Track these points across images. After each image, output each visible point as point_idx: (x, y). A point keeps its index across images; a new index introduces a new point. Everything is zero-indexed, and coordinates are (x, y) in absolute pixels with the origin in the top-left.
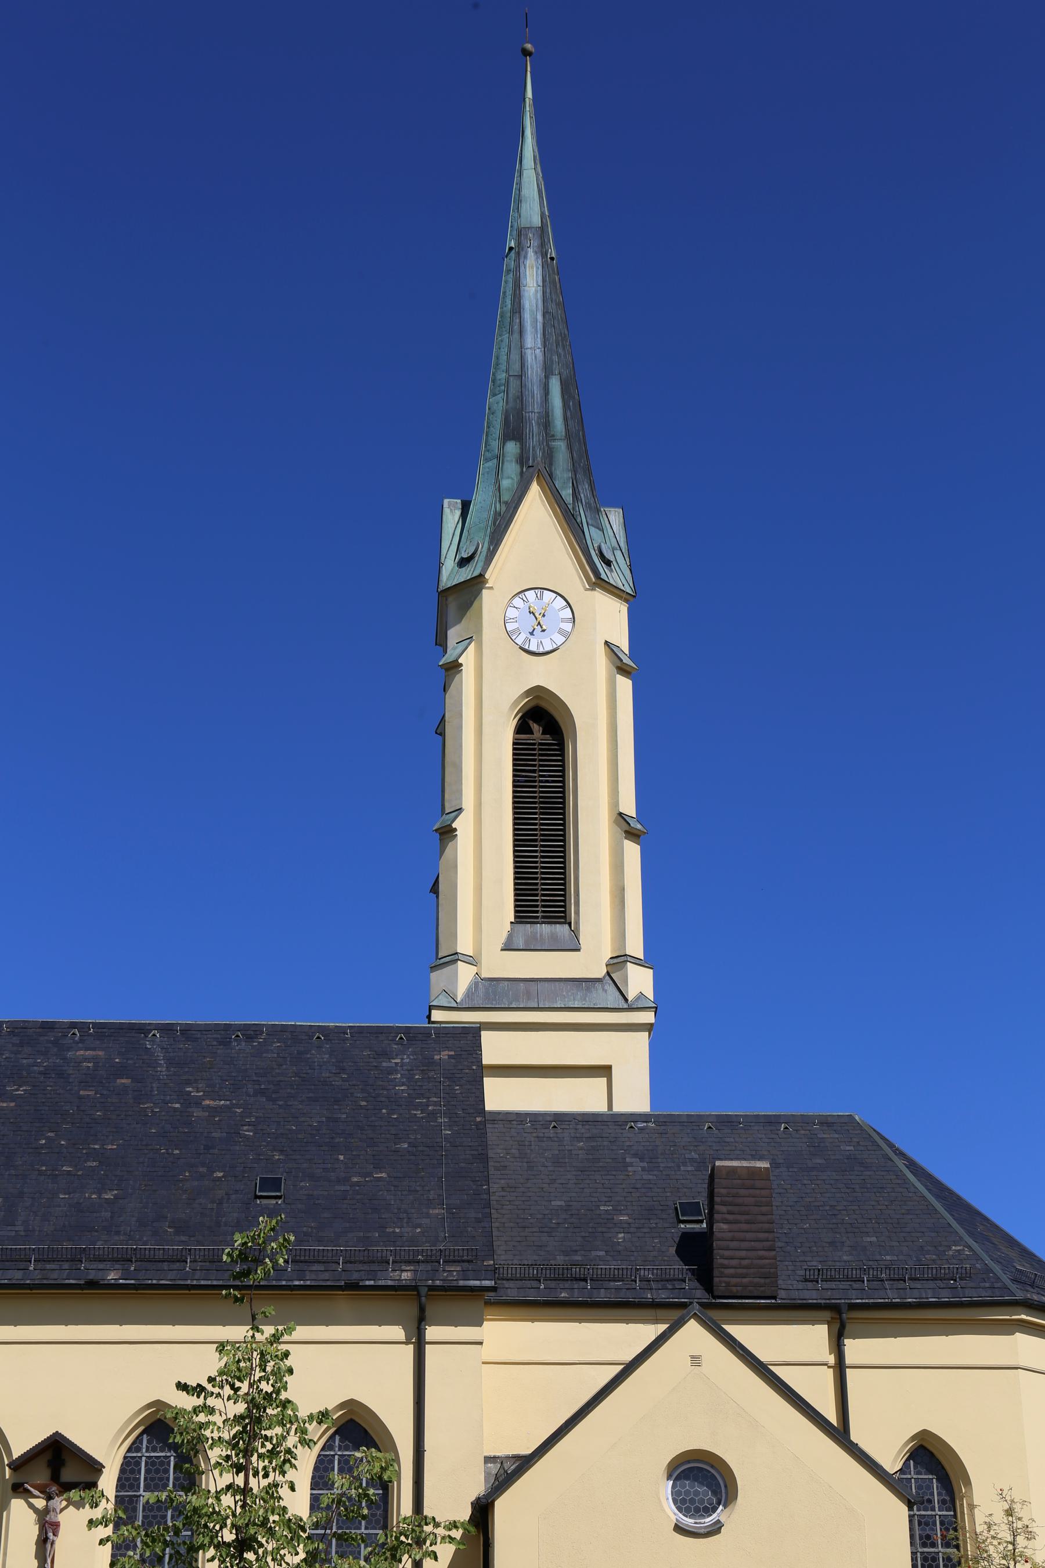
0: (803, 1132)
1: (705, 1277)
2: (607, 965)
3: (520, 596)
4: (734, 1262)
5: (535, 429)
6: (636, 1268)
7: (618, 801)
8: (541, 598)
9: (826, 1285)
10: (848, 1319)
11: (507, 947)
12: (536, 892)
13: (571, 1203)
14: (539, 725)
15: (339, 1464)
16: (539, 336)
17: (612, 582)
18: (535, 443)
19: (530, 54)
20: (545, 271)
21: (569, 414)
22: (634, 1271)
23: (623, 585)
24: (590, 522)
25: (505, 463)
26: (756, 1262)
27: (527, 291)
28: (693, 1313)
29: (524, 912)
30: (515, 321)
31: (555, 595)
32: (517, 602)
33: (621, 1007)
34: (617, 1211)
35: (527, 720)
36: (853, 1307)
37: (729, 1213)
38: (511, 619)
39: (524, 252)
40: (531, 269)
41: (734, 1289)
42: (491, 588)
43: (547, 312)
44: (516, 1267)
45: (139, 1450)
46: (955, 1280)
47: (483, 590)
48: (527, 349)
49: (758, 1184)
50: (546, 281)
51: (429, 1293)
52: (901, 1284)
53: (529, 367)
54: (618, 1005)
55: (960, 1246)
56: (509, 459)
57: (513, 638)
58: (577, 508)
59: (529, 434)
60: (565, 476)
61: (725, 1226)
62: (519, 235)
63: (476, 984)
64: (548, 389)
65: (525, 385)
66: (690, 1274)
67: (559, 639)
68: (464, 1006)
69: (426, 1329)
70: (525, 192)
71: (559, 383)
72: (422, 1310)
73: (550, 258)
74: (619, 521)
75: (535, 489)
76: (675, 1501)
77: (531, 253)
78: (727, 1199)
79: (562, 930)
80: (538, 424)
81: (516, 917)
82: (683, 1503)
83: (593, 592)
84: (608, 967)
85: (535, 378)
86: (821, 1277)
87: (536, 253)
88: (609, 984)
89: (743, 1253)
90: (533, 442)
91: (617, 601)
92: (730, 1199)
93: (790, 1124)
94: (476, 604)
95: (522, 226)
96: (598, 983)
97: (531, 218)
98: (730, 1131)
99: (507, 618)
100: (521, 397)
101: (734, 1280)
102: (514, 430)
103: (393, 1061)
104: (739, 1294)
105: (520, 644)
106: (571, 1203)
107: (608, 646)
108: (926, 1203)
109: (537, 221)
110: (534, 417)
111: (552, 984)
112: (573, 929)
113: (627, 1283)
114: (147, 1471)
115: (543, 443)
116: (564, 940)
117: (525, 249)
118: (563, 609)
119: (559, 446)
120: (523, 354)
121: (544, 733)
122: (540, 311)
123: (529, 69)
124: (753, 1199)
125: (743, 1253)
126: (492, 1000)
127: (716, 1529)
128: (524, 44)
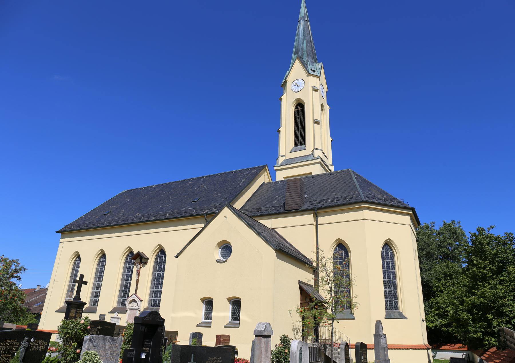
21: (307, 46)
29: (297, 144)
32: (294, 83)
36: (318, 209)
42: (288, 82)
49: (297, 182)
51: (207, 215)
67: (302, 88)
75: (297, 61)
76: (221, 255)
77: (302, 21)
79: (303, 146)
83: (308, 77)
87: (303, 20)
89: (292, 199)
101: (289, 206)
102: (296, 53)
111: (300, 158)
114: (159, 260)
125: (292, 199)
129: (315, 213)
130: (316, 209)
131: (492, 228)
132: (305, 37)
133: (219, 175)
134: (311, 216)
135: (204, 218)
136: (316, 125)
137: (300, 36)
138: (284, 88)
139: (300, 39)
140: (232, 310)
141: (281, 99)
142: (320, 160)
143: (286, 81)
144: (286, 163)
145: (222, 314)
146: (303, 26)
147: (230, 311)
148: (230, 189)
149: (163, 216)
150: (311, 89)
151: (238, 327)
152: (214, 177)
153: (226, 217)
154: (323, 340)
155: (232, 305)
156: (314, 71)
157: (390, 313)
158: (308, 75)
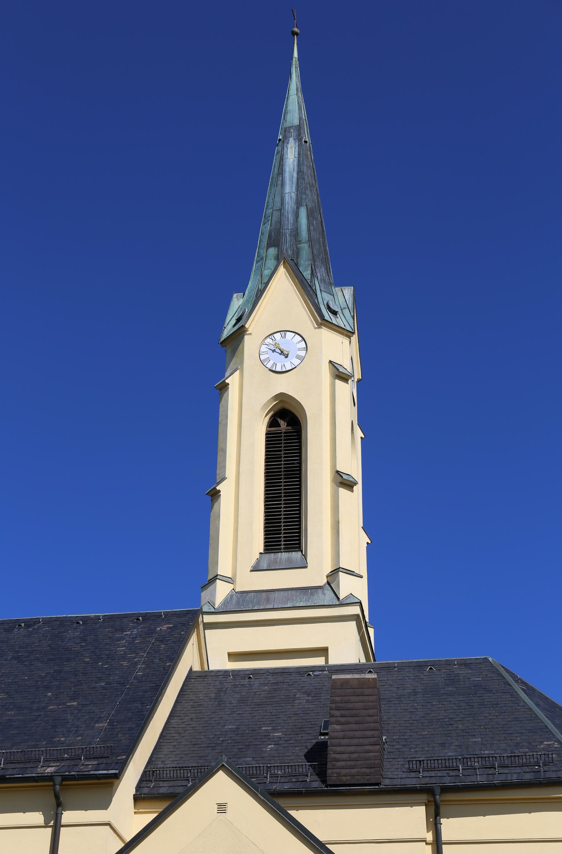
0: (444, 671)
1: (322, 774)
2: (327, 577)
3: (270, 337)
4: (344, 756)
5: (288, 238)
6: (267, 766)
7: (336, 463)
8: (285, 337)
9: (426, 774)
10: (442, 801)
11: (256, 569)
12: (280, 532)
13: (239, 727)
14: (285, 421)
16: (294, 185)
17: (334, 322)
18: (287, 246)
19: (297, 34)
20: (300, 149)
22: (265, 768)
23: (345, 326)
24: (323, 289)
25: (267, 261)
26: (362, 755)
27: (288, 161)
28: (221, 765)
30: (279, 179)
31: (294, 334)
32: (268, 341)
33: (334, 604)
34: (275, 730)
35: (276, 418)
36: (445, 790)
37: (342, 716)
38: (263, 352)
39: (287, 140)
40: (291, 150)
41: (344, 778)
42: (250, 334)
43: (300, 171)
44: (170, 770)
46: (539, 766)
47: (245, 336)
48: (286, 194)
49: (367, 691)
50: (300, 154)
51: (64, 783)
52: (491, 771)
53: (287, 203)
54: (332, 603)
55: (552, 741)
56: (269, 258)
57: (265, 364)
58: (313, 281)
59: (284, 242)
60: (307, 263)
61: (338, 727)
62: (285, 131)
63: (232, 596)
64: (298, 214)
65: (283, 214)
67: (296, 362)
68: (220, 611)
69: (63, 814)
70: (290, 108)
71: (306, 211)
72: (57, 797)
73: (304, 142)
74: (350, 293)
75: (282, 270)
77: (291, 140)
78: (340, 705)
79: (296, 555)
80: (291, 235)
81: (265, 550)
83: (320, 330)
84: (328, 578)
85: (290, 209)
86: (422, 766)
88: (328, 589)
89: (352, 749)
90: (286, 246)
91: (341, 337)
92: (343, 705)
93: (435, 666)
94: (241, 346)
95: (287, 126)
96: (319, 589)
97: (293, 121)
98: (386, 673)
99: (261, 352)
100: (280, 222)
101: (344, 771)
103: (125, 633)
104: (348, 783)
105: (269, 367)
106: (239, 727)
107: (331, 363)
108: (530, 713)
109: (296, 122)
110: (288, 232)
111: (286, 593)
112: (303, 554)
113: (261, 779)
115: (293, 246)
116: (296, 562)
117: (288, 138)
118: (299, 342)
119: (303, 247)
120: (283, 197)
121: (287, 426)
122: (296, 171)
123: (296, 42)
124: (362, 704)
125: (352, 749)
126: (241, 605)
128: (293, 28)
129: (435, 801)
130: (438, 791)
132: (304, 196)
134: (420, 811)
136: (343, 492)
137: (287, 189)
139: (287, 198)
141: (224, 387)
142: (356, 610)
144: (238, 603)
146: (296, 160)
148: (103, 688)
150: (326, 373)
153: (222, 808)
156: (335, 313)
158: (320, 325)
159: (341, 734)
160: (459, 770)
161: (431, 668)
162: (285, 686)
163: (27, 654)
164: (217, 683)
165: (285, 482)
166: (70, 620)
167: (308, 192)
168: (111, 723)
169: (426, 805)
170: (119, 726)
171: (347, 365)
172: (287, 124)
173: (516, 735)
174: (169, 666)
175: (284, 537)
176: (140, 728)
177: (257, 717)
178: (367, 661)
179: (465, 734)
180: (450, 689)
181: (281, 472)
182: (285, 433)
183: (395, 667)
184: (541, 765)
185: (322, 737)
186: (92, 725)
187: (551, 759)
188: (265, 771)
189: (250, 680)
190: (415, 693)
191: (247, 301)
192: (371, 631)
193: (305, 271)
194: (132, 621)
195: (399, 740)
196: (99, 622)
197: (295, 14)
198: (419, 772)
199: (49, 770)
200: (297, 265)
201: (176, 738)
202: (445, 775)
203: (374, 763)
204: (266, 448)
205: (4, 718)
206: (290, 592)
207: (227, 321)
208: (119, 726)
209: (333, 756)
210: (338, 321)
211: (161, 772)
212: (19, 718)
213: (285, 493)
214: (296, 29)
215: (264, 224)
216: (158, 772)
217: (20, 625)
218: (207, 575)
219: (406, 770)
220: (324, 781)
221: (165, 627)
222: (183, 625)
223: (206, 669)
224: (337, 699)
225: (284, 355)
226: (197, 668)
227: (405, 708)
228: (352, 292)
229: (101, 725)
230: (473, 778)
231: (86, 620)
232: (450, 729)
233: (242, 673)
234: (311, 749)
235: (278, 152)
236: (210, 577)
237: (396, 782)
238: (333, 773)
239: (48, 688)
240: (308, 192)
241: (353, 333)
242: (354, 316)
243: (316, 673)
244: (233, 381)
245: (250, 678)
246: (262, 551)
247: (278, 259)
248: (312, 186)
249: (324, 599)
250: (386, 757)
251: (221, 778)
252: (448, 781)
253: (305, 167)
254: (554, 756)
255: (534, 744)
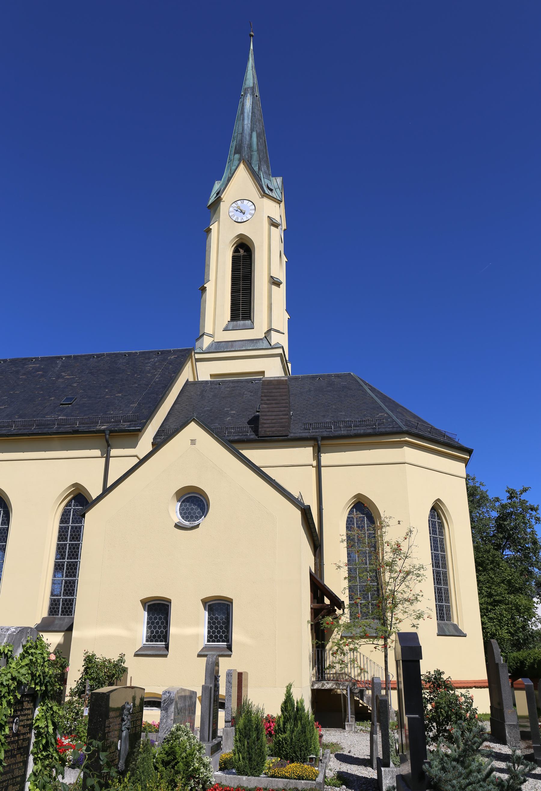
1: (256, 431)
2: (265, 334)
4: (268, 421)
8: (243, 203)
10: (321, 445)
14: (243, 250)
15: (73, 513)
17: (271, 194)
19: (253, 36)
24: (265, 177)
29: (235, 316)
31: (248, 201)
32: (234, 205)
34: (232, 410)
36: (324, 438)
37: (268, 400)
41: (268, 433)
42: (224, 201)
45: (70, 506)
49: (281, 387)
51: (111, 434)
61: (265, 406)
62: (245, 90)
63: (212, 344)
66: (250, 429)
67: (249, 217)
70: (248, 77)
72: (107, 441)
75: (242, 166)
76: (181, 514)
77: (249, 95)
79: (248, 322)
80: (247, 147)
82: (185, 514)
83: (263, 199)
86: (312, 427)
87: (250, 95)
89: (273, 417)
94: (219, 208)
100: (241, 140)
101: (268, 429)
104: (270, 435)
109: (251, 85)
111: (242, 342)
118: (251, 206)
121: (244, 252)
123: (252, 40)
125: (273, 417)
127: (197, 526)
129: (318, 445)
130: (320, 439)
131: (525, 490)
132: (255, 126)
133: (34, 360)
134: (310, 450)
135: (105, 439)
136: (274, 288)
137: (246, 122)
138: (212, 212)
139: (246, 127)
140: (209, 623)
141: (209, 231)
142: (280, 351)
143: (218, 201)
144: (216, 348)
145: (190, 631)
146: (251, 106)
147: (205, 626)
148: (136, 387)
149: (4, 429)
151: (230, 656)
152: (86, 359)
153: (193, 442)
154: (331, 675)
155: (208, 613)
156: (271, 190)
157: (443, 627)
158: (263, 197)
159: (267, 410)
160: (332, 428)
161: (319, 379)
162: (238, 388)
163: (96, 371)
164: (202, 387)
165: (242, 283)
166: (121, 354)
167: (257, 124)
168: (139, 404)
169: (313, 447)
170: (143, 406)
171: (278, 219)
172: (246, 86)
173: (364, 410)
174: (173, 376)
175: (242, 313)
176: (155, 406)
177: (222, 404)
178: (285, 375)
179: (336, 411)
180: (329, 389)
181: (240, 277)
182: (243, 256)
183: (300, 378)
184: (377, 425)
185: (258, 413)
186: (129, 405)
187: (382, 422)
188: (225, 430)
189: (220, 385)
190: (310, 391)
191: (223, 184)
192: (289, 365)
193: (255, 167)
194: (155, 354)
195: (300, 414)
196: (137, 355)
197: (252, 25)
198: (310, 430)
199: (103, 427)
200: (250, 164)
201: (177, 414)
202: (324, 431)
203: (285, 425)
204: (232, 264)
205: (81, 402)
206: (244, 342)
207: (212, 195)
208: (143, 406)
209: (262, 421)
210: (273, 194)
211: (168, 431)
212: (89, 402)
213: (242, 289)
214: (252, 33)
215: (233, 142)
216: (166, 431)
217: (94, 357)
218: (199, 333)
219: (303, 429)
220: (257, 435)
221: (172, 357)
222: (183, 356)
223: (197, 380)
224: (265, 391)
225: (243, 213)
226: (191, 379)
227: (305, 398)
228: (281, 180)
229: (134, 405)
230: (339, 432)
231: (129, 354)
232: (328, 408)
233: (215, 382)
234: (251, 419)
235: (241, 102)
236: (200, 334)
237: (296, 435)
238: (262, 430)
239: (106, 387)
240: (257, 124)
241: (281, 201)
242: (282, 192)
243: (256, 382)
244: (214, 227)
245: (220, 384)
246: (229, 319)
247: (240, 160)
248: (260, 121)
249: (263, 345)
250: (292, 422)
251: (193, 425)
252: (325, 434)
253: (256, 110)
254: (384, 420)
255: (373, 415)
